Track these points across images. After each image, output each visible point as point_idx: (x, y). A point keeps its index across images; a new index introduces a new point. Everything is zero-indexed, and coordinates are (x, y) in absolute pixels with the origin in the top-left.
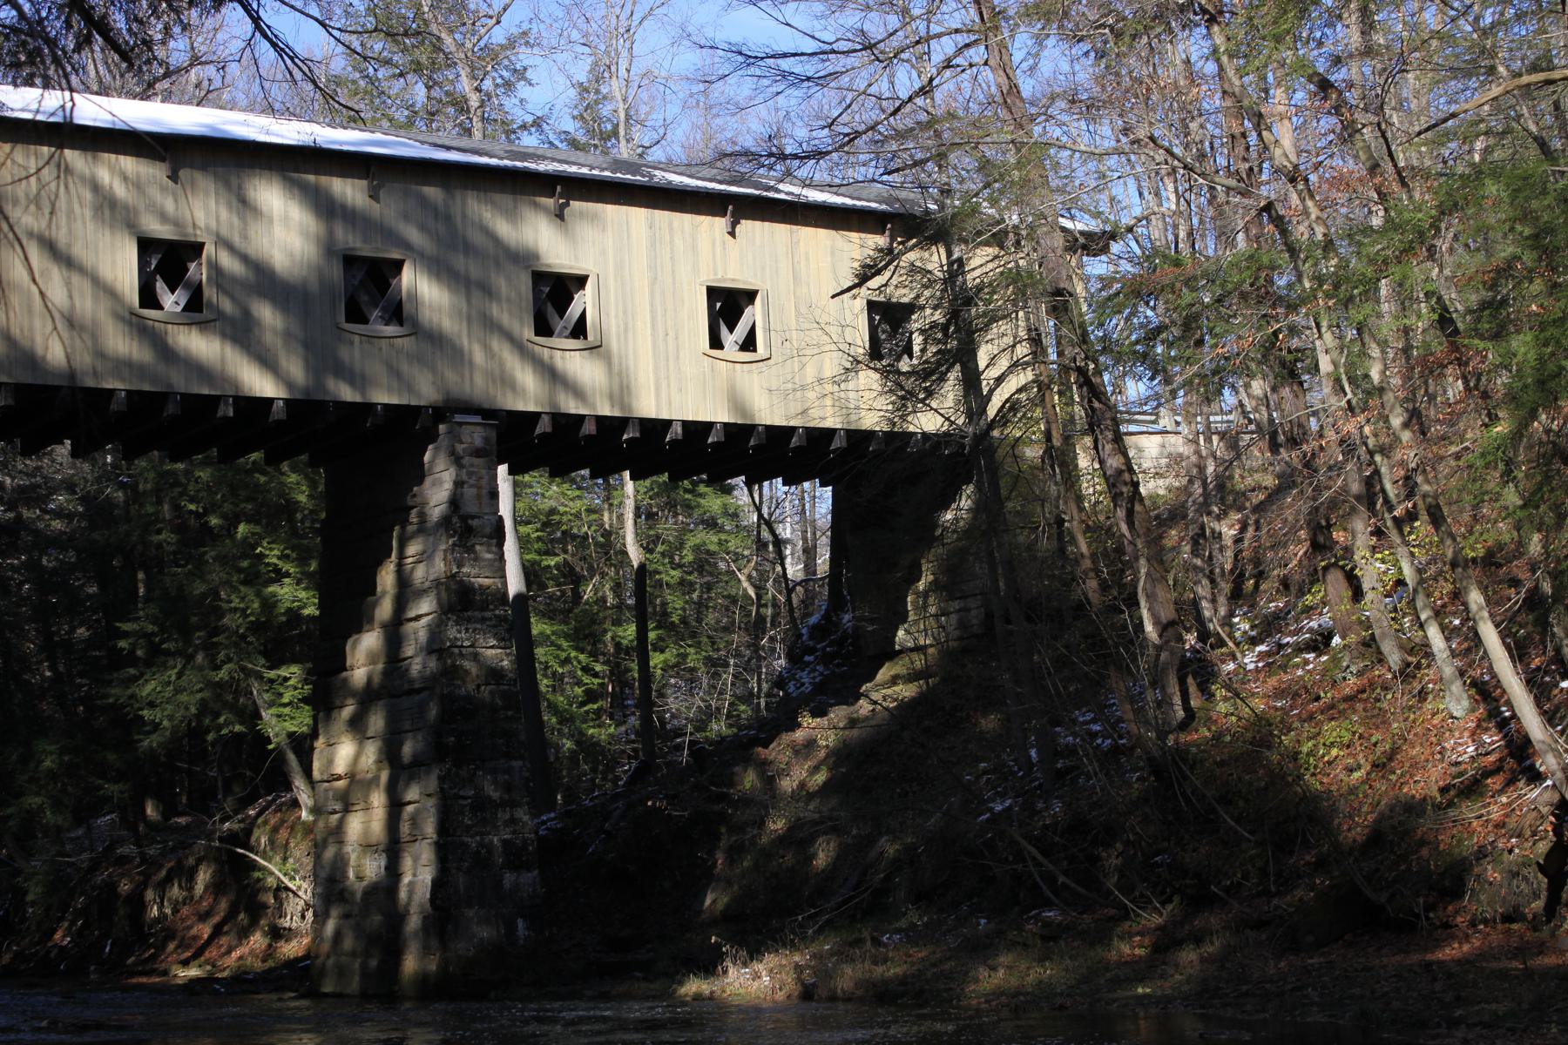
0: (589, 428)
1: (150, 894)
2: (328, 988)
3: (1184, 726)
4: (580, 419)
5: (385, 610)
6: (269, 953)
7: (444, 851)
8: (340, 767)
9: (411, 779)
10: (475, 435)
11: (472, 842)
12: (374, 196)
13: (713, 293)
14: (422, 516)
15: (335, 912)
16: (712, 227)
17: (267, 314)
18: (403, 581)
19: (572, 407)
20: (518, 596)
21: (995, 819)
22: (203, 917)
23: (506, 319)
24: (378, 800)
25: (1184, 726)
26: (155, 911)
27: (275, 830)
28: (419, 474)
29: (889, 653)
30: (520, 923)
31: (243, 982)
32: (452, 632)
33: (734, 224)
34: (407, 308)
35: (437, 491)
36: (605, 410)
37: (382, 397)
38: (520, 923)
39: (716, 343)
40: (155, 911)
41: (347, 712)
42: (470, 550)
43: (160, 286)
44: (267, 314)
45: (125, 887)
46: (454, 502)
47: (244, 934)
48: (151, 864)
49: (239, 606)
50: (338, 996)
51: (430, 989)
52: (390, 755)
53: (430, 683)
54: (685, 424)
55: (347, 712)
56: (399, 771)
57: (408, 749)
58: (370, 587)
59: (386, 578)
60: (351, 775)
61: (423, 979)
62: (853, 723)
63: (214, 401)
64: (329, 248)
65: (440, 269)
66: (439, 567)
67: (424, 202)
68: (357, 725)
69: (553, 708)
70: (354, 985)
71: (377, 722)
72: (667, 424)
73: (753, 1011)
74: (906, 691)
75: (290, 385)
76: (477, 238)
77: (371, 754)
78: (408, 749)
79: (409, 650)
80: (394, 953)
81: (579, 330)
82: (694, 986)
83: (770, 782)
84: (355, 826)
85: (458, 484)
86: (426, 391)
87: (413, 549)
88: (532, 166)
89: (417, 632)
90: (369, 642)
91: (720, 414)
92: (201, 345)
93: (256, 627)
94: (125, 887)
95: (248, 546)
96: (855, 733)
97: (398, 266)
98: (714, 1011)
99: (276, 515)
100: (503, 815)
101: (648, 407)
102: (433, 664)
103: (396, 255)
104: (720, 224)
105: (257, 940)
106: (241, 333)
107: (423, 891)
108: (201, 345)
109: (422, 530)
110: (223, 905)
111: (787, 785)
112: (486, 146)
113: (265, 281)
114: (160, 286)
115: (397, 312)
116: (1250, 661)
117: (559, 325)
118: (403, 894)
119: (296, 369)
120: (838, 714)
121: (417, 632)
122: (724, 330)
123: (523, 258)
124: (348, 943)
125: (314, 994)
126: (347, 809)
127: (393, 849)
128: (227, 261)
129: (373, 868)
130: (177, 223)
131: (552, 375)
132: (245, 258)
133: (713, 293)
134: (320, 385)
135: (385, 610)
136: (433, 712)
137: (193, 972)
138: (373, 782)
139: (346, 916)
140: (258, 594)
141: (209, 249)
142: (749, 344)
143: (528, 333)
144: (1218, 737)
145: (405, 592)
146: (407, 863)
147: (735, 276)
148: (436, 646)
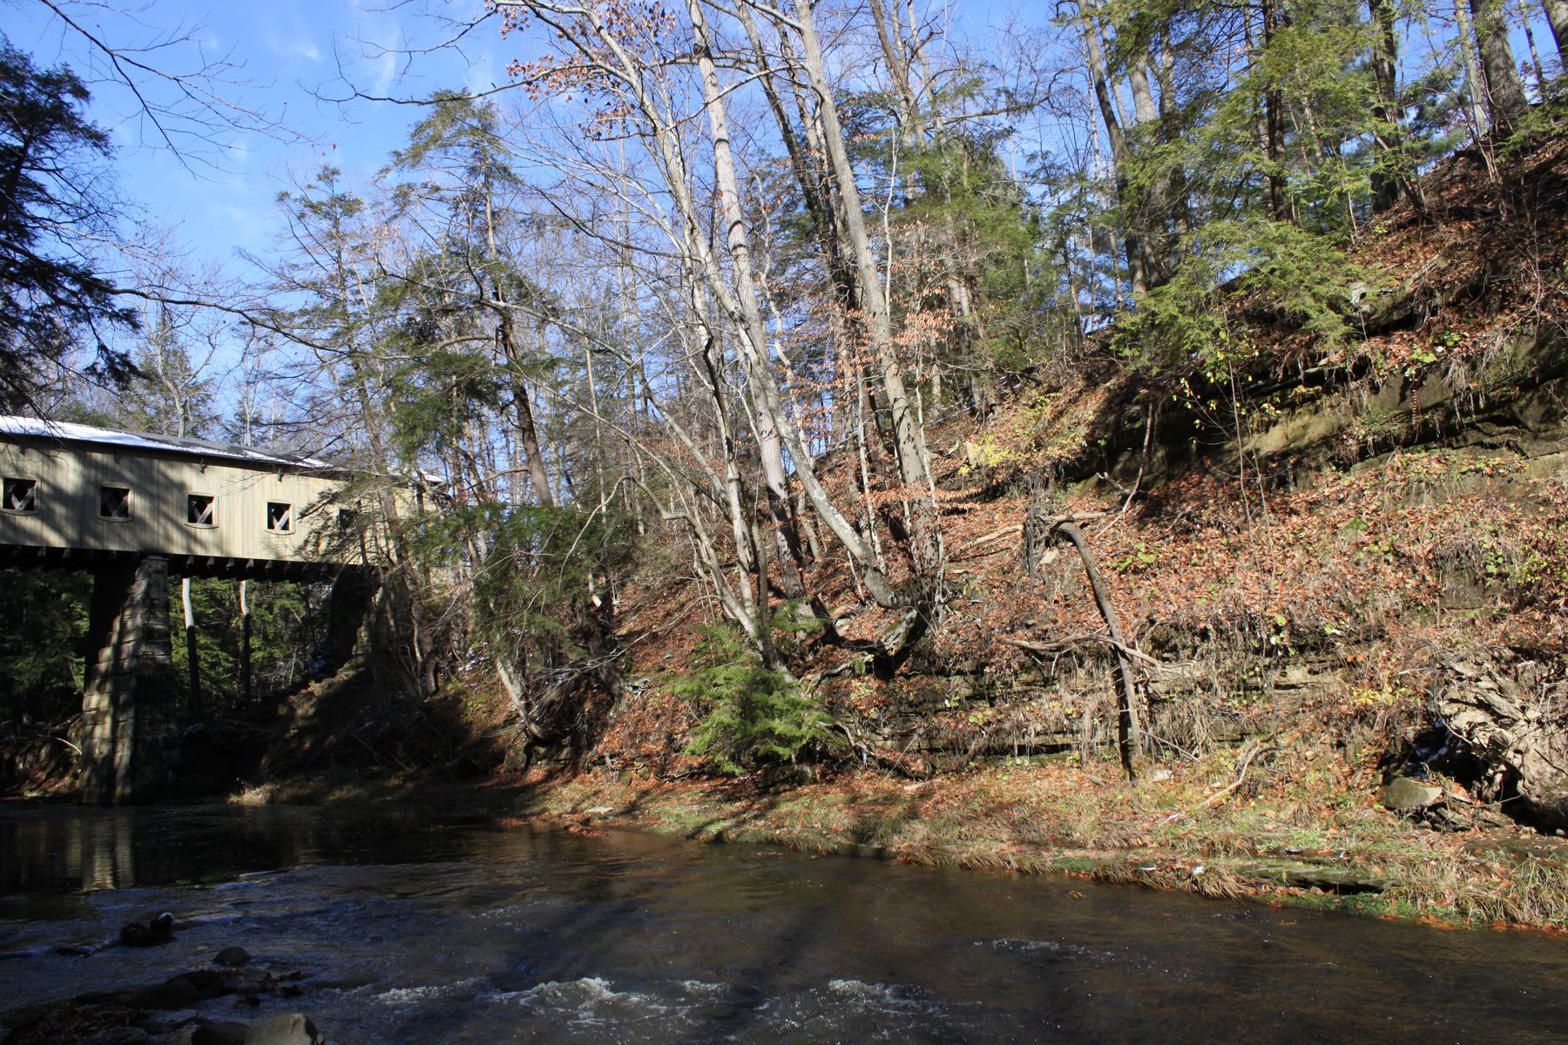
0: (210, 562)
1: (18, 759)
2: (85, 801)
3: (435, 693)
4: (207, 558)
5: (115, 638)
6: (72, 784)
7: (136, 742)
8: (93, 705)
9: (123, 712)
10: (159, 565)
11: (149, 738)
12: (117, 461)
13: (270, 505)
14: (133, 599)
15: (89, 768)
16: (271, 478)
17: (60, 510)
18: (123, 624)
19: (200, 552)
20: (190, 628)
21: (366, 729)
22: (43, 769)
23: (173, 514)
24: (108, 720)
25: (435, 693)
26: (21, 766)
27: (78, 730)
28: (133, 581)
29: (349, 657)
30: (170, 773)
31: (57, 798)
32: (143, 648)
33: (281, 476)
34: (130, 510)
35: (140, 588)
36: (217, 554)
37: (114, 547)
38: (170, 773)
39: (271, 526)
40: (21, 766)
41: (97, 681)
42: (154, 614)
43: (14, 499)
44: (60, 510)
45: (7, 756)
46: (147, 593)
47: (62, 777)
48: (20, 744)
49: (64, 630)
50: (88, 804)
51: (125, 801)
52: (114, 701)
53: (132, 670)
54: (255, 560)
55: (97, 681)
56: (117, 707)
57: (122, 698)
58: (111, 628)
59: (117, 625)
60: (97, 709)
61: (122, 796)
62: (330, 686)
63: (36, 549)
64: (87, 481)
65: (141, 491)
66: (139, 621)
67: (139, 464)
68: (100, 689)
69: (208, 677)
70: (94, 800)
71: (108, 687)
72: (247, 560)
73: (255, 808)
74: (351, 673)
75: (67, 539)
76: (161, 479)
77: (105, 703)
78: (122, 698)
79: (124, 655)
80: (112, 786)
81: (209, 520)
82: (234, 799)
83: (293, 710)
84: (98, 731)
85: (149, 585)
86: (133, 547)
87: (128, 613)
88: (191, 450)
89: (128, 647)
90: (107, 652)
91: (270, 557)
92: (30, 523)
93: (71, 639)
94: (7, 756)
95: (67, 603)
96: (331, 691)
97: (126, 492)
98: (240, 809)
99: (79, 591)
100: (164, 726)
101: (238, 552)
102: (135, 662)
103: (125, 487)
104: (276, 476)
105: (67, 779)
106: (47, 518)
107: (126, 760)
108: (30, 523)
109: (132, 606)
110: (53, 764)
111: (300, 712)
112: (169, 438)
113: (58, 494)
114: (14, 499)
115: (124, 511)
116: (468, 667)
117: (200, 517)
118: (117, 760)
119: (71, 532)
120: (325, 682)
121: (128, 647)
122: (275, 521)
123: (181, 486)
124: (94, 781)
125: (80, 804)
126: (95, 724)
127: (113, 741)
128: (45, 488)
129: (105, 749)
130: (17, 469)
131: (192, 537)
132: (48, 484)
133: (270, 505)
134: (81, 540)
135: (115, 638)
136: (133, 683)
137: (34, 794)
138: (105, 713)
139: (93, 770)
140: (71, 625)
141: (38, 484)
142: (285, 527)
143: (184, 521)
144: (446, 698)
145: (123, 633)
146: (120, 747)
147: (280, 499)
148: (134, 655)
